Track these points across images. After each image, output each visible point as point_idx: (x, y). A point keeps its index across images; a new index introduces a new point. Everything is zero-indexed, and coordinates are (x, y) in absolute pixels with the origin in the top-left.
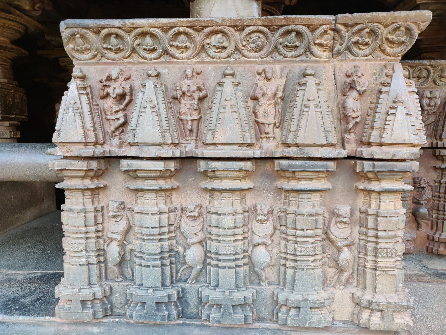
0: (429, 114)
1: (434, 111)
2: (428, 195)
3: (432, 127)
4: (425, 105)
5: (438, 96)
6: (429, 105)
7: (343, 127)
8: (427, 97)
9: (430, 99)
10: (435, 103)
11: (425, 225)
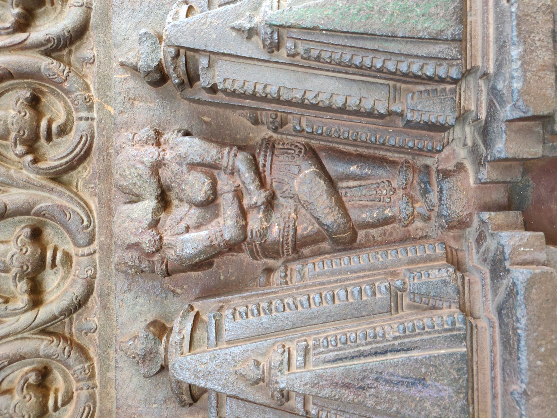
0: (270, 204)
1: (247, 175)
3: (353, 169)
4: (203, 233)
5: (150, 153)
6: (210, 203)
7: (225, 346)
8: (155, 224)
9: (164, 200)
10: (193, 166)
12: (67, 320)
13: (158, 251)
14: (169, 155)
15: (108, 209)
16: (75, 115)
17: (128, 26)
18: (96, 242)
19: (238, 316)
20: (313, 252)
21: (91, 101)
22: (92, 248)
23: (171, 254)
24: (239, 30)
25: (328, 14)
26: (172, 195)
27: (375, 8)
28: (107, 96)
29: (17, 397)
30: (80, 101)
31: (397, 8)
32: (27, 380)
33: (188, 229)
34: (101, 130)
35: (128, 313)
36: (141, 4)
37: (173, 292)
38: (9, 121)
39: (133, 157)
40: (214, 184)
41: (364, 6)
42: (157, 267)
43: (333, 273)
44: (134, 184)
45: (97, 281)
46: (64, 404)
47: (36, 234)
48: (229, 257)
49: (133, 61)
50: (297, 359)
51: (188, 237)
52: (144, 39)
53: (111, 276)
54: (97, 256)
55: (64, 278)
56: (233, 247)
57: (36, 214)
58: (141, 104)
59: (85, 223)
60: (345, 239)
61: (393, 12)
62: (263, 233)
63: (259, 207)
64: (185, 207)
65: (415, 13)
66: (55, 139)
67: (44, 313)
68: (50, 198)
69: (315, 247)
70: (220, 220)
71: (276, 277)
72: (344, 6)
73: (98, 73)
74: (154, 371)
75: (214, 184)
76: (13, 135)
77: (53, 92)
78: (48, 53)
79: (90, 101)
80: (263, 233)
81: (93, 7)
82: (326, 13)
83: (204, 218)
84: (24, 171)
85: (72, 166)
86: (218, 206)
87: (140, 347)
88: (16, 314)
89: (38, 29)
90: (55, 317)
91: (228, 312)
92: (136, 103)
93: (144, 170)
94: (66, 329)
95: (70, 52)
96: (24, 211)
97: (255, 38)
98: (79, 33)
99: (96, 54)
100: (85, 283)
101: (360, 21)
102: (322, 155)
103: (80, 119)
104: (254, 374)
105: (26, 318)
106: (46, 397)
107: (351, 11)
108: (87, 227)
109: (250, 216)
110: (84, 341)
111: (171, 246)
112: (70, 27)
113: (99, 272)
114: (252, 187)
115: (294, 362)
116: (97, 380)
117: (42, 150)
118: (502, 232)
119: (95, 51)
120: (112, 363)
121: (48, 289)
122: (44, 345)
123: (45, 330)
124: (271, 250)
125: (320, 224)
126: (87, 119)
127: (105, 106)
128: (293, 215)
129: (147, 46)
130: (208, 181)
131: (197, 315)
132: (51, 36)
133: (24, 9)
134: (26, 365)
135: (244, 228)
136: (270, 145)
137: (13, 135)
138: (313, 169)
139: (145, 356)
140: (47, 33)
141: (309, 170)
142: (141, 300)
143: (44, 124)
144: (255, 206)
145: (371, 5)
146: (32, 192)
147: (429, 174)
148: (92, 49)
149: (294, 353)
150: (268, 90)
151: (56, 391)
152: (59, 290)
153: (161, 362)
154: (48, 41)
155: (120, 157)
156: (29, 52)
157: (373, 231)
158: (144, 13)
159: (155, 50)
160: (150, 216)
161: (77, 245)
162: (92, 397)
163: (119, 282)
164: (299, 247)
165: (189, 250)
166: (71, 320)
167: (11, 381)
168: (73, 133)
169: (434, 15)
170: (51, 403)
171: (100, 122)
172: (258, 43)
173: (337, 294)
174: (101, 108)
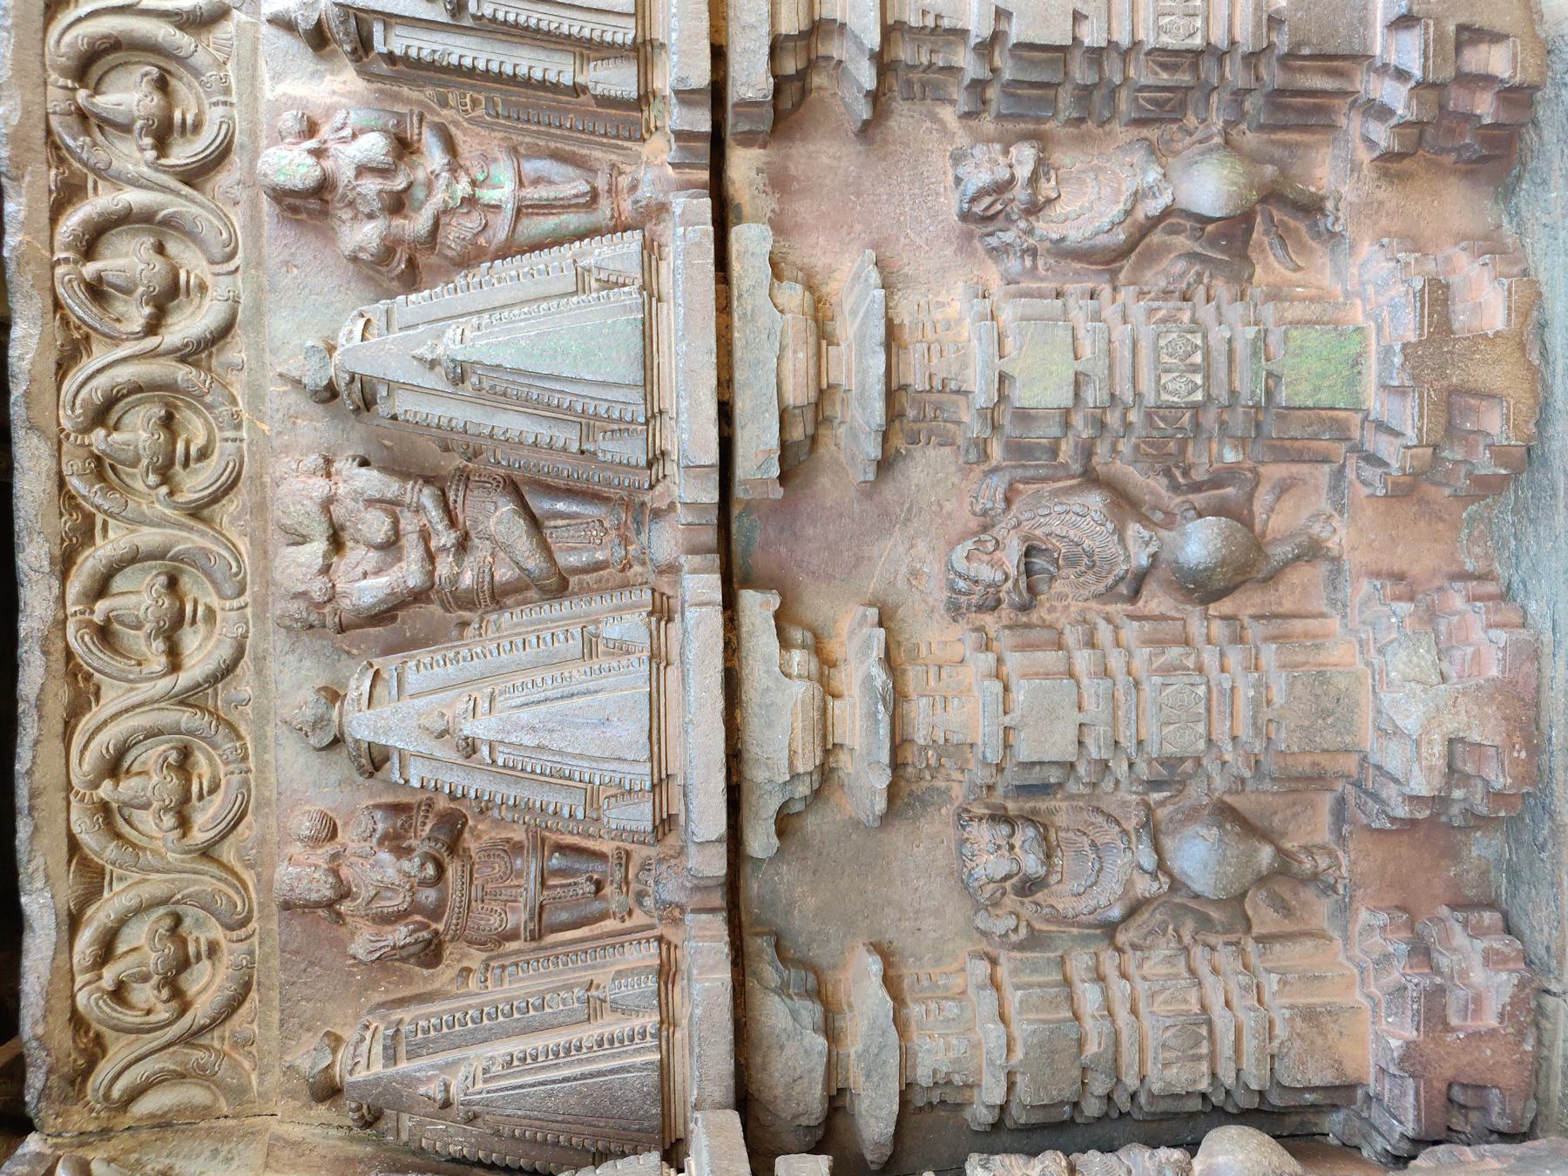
0: (463, 546)
1: (435, 513)
2: (1085, 524)
3: (560, 506)
5: (319, 487)
6: (391, 546)
8: (326, 569)
9: (336, 542)
10: (370, 502)
11: (1288, 503)
12: (210, 691)
13: (330, 600)
14: (342, 490)
15: (263, 551)
16: (218, 435)
18: (248, 593)
19: (422, 671)
20: (904, 741)
22: (242, 601)
23: (345, 604)
24: (421, 360)
26: (346, 536)
29: (155, 779)
32: (166, 759)
33: (365, 575)
34: (252, 455)
35: (291, 680)
37: (348, 653)
38: (141, 446)
39: (298, 490)
40: (396, 523)
42: (329, 621)
43: (532, 623)
44: (301, 523)
45: (249, 642)
46: (211, 792)
47: (173, 584)
48: (414, 610)
49: (296, 374)
50: (483, 705)
51: (364, 583)
53: (267, 635)
54: (249, 610)
55: (207, 638)
56: (419, 596)
57: (172, 559)
59: (234, 569)
60: (558, 586)
62: (455, 579)
63: (448, 550)
64: (362, 550)
66: (192, 465)
67: (184, 679)
68: (190, 539)
69: (520, 597)
70: (403, 564)
71: (469, 632)
74: (326, 741)
75: (396, 523)
76: (145, 462)
77: (189, 406)
78: (183, 360)
80: (455, 579)
83: (384, 562)
84: (157, 506)
85: (215, 499)
86: (401, 548)
87: (309, 713)
88: (151, 679)
89: (171, 329)
90: (199, 685)
91: (412, 664)
93: (314, 509)
94: (210, 701)
96: (158, 555)
97: (438, 369)
98: (224, 332)
100: (235, 644)
102: (525, 489)
103: (226, 440)
104: (439, 725)
105: (164, 684)
106: (189, 781)
108: (237, 574)
109: (438, 561)
110: (233, 717)
111: (345, 595)
112: (212, 327)
113: (251, 630)
114: (440, 527)
115: (479, 710)
116: (252, 764)
117: (177, 479)
120: (271, 742)
121: (186, 652)
122: (185, 718)
123: (185, 699)
124: (466, 601)
125: (520, 568)
126: (234, 440)
128: (489, 559)
129: (314, 362)
130: (388, 521)
131: (377, 673)
133: (156, 306)
134: (163, 743)
135: (431, 573)
136: (464, 477)
137: (145, 462)
138: (511, 506)
139: (315, 723)
141: (507, 507)
142: (307, 663)
143: (180, 447)
144: (444, 549)
146: (169, 531)
147: (643, 513)
149: (479, 701)
150: (454, 423)
151: (200, 777)
152: (202, 652)
153: (334, 730)
154: (187, 345)
155: (283, 490)
156: (162, 360)
157: (587, 577)
160: (320, 561)
161: (222, 596)
162: (246, 783)
163: (278, 641)
164: (498, 596)
165: (367, 600)
166: (216, 691)
167: (144, 763)
168: (215, 457)
170: (195, 788)
171: (251, 444)
174: (253, 427)
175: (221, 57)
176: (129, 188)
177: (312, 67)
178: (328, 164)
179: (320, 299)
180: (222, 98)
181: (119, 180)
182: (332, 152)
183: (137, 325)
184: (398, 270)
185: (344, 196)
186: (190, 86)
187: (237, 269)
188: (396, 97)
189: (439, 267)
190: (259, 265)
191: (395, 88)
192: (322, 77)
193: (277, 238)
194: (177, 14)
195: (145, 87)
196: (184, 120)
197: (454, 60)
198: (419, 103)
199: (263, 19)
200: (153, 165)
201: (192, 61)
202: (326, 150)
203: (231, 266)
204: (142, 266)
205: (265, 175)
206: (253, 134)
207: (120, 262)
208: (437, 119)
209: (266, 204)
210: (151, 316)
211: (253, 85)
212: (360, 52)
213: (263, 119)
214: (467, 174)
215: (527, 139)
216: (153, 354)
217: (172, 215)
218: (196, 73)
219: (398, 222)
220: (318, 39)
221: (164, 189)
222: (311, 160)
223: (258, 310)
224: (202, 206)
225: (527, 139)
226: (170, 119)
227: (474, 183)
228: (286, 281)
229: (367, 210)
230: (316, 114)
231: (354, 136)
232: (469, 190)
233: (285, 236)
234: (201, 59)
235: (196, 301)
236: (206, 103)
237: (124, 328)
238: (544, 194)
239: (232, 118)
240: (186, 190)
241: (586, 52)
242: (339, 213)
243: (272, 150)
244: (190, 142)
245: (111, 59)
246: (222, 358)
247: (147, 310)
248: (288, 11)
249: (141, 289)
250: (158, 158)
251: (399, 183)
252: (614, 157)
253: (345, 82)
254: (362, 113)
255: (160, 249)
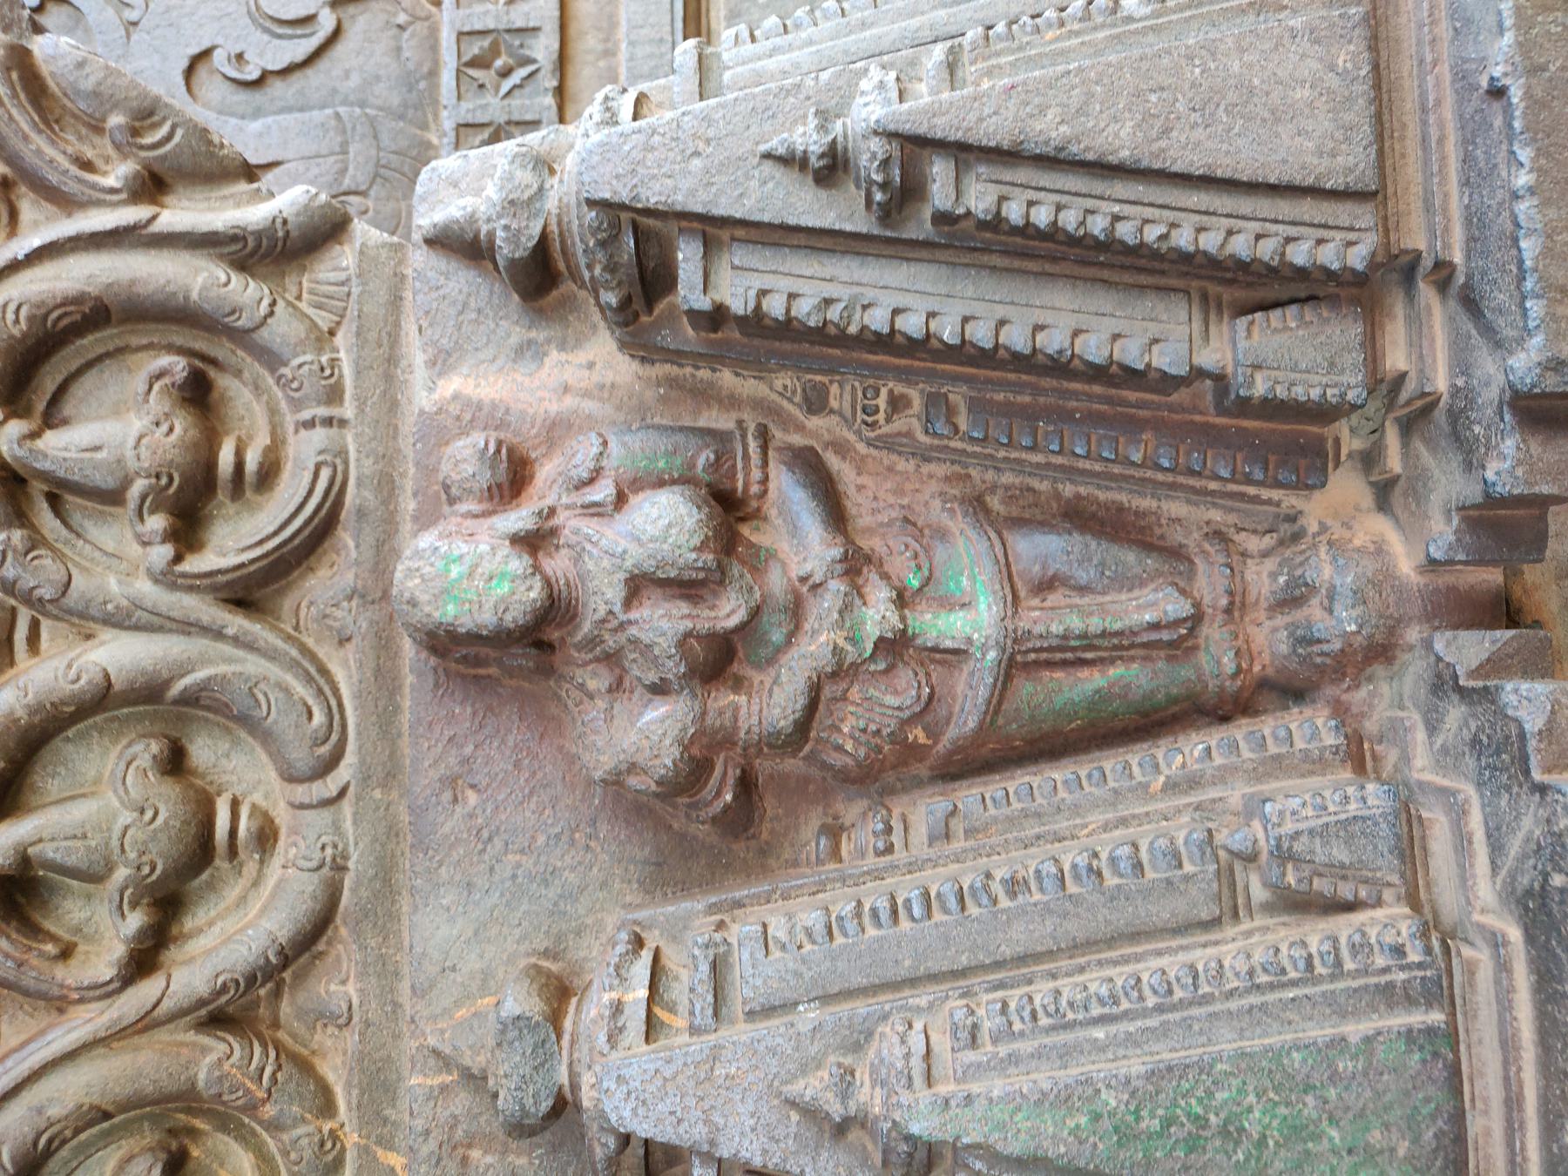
17: (455, 932)
21: (338, 1146)
25: (1078, 1126)
27: (1212, 1118)
28: (385, 1120)
30: (308, 1154)
31: (1275, 1124)
36: (492, 869)
41: (1179, 1111)
52: (512, 1034)
58: (489, 1159)
61: (1265, 1136)
65: (1325, 1144)
72: (1123, 1107)
73: (361, 1057)
79: (334, 1145)
81: (351, 864)
82: (1071, 1123)
89: (195, 946)
92: (475, 1154)
95: (277, 994)
99: (355, 1002)
101: (1169, 1154)
107: (1143, 1125)
118: (1408, 576)
119: (351, 988)
127: (380, 1152)
132: (229, 976)
140: (220, 968)
145: (1199, 1110)
148: (344, 982)
156: (163, 1035)
158: (502, 895)
159: (542, 1064)
169: (1381, 1152)
172: (865, 1148)
173: (939, 895)
175: (324, 320)
176: (107, 634)
177: (518, 334)
178: (558, 564)
179: (528, 862)
180: (322, 411)
181: (89, 620)
182: (566, 535)
183: (102, 962)
184: (718, 806)
185: (592, 642)
186: (257, 388)
187: (342, 793)
188: (704, 395)
189: (806, 780)
190: (391, 775)
191: (704, 374)
192: (540, 356)
193: (435, 730)
194: (234, 238)
195: (158, 403)
196: (239, 466)
197: (878, 320)
198: (758, 404)
199: (417, 237)
200: (168, 578)
201: (264, 335)
202: (554, 532)
203: (331, 785)
204: (126, 817)
205: (413, 603)
206: (387, 485)
207: (78, 812)
208: (797, 440)
209: (408, 648)
210: (142, 934)
211: (389, 378)
212: (638, 304)
213: (410, 453)
214: (885, 577)
215: (1008, 478)
216: (147, 1023)
217: (204, 686)
218: (271, 359)
219: (723, 699)
220: (538, 277)
221: (188, 627)
222: (518, 564)
223: (385, 875)
224: (271, 655)
225: (1008, 478)
226: (211, 465)
227: (902, 600)
228: (451, 823)
229: (652, 677)
230: (528, 438)
231: (621, 500)
232: (894, 619)
233: (451, 718)
234: (283, 330)
235: (250, 868)
236: (289, 420)
237: (72, 975)
238: (1076, 623)
239: (343, 453)
240: (236, 623)
241: (1213, 289)
242: (581, 675)
243: (426, 540)
244: (252, 509)
245: (90, 344)
246: (301, 997)
247: (135, 921)
248: (472, 219)
249: (121, 873)
250: (178, 559)
251: (728, 611)
252: (1216, 515)
253: (591, 365)
254: (636, 441)
255: (175, 762)
